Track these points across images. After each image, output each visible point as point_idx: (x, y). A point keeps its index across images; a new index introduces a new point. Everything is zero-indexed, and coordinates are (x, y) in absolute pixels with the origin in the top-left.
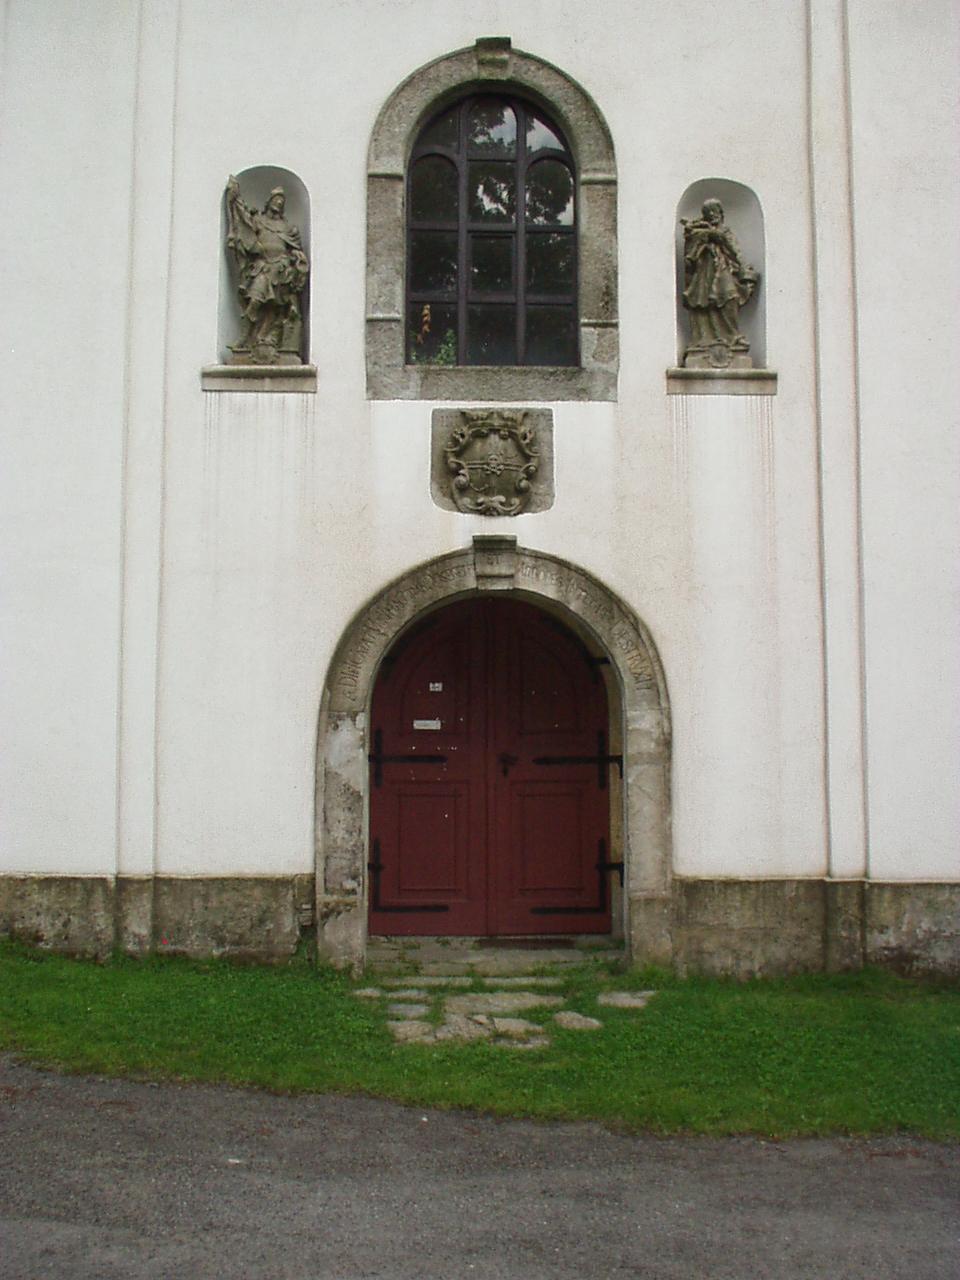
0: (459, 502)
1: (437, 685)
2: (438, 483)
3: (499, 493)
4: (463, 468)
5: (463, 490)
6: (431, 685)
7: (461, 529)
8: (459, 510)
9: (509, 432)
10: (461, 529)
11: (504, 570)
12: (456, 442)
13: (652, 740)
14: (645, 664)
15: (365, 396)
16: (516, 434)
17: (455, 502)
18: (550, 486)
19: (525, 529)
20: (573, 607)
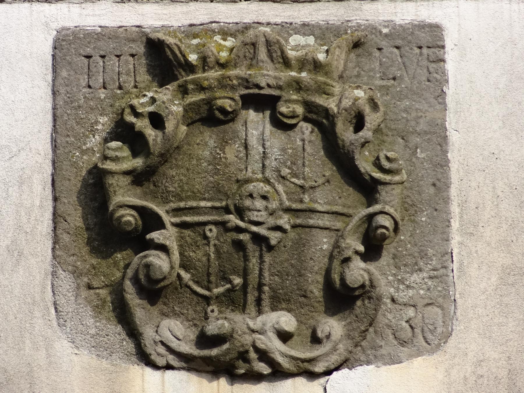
0: (148, 334)
2: (77, 273)
4: (161, 226)
5: (153, 290)
8: (145, 359)
9: (309, 106)
12: (124, 132)
17: (133, 333)
18: (441, 275)
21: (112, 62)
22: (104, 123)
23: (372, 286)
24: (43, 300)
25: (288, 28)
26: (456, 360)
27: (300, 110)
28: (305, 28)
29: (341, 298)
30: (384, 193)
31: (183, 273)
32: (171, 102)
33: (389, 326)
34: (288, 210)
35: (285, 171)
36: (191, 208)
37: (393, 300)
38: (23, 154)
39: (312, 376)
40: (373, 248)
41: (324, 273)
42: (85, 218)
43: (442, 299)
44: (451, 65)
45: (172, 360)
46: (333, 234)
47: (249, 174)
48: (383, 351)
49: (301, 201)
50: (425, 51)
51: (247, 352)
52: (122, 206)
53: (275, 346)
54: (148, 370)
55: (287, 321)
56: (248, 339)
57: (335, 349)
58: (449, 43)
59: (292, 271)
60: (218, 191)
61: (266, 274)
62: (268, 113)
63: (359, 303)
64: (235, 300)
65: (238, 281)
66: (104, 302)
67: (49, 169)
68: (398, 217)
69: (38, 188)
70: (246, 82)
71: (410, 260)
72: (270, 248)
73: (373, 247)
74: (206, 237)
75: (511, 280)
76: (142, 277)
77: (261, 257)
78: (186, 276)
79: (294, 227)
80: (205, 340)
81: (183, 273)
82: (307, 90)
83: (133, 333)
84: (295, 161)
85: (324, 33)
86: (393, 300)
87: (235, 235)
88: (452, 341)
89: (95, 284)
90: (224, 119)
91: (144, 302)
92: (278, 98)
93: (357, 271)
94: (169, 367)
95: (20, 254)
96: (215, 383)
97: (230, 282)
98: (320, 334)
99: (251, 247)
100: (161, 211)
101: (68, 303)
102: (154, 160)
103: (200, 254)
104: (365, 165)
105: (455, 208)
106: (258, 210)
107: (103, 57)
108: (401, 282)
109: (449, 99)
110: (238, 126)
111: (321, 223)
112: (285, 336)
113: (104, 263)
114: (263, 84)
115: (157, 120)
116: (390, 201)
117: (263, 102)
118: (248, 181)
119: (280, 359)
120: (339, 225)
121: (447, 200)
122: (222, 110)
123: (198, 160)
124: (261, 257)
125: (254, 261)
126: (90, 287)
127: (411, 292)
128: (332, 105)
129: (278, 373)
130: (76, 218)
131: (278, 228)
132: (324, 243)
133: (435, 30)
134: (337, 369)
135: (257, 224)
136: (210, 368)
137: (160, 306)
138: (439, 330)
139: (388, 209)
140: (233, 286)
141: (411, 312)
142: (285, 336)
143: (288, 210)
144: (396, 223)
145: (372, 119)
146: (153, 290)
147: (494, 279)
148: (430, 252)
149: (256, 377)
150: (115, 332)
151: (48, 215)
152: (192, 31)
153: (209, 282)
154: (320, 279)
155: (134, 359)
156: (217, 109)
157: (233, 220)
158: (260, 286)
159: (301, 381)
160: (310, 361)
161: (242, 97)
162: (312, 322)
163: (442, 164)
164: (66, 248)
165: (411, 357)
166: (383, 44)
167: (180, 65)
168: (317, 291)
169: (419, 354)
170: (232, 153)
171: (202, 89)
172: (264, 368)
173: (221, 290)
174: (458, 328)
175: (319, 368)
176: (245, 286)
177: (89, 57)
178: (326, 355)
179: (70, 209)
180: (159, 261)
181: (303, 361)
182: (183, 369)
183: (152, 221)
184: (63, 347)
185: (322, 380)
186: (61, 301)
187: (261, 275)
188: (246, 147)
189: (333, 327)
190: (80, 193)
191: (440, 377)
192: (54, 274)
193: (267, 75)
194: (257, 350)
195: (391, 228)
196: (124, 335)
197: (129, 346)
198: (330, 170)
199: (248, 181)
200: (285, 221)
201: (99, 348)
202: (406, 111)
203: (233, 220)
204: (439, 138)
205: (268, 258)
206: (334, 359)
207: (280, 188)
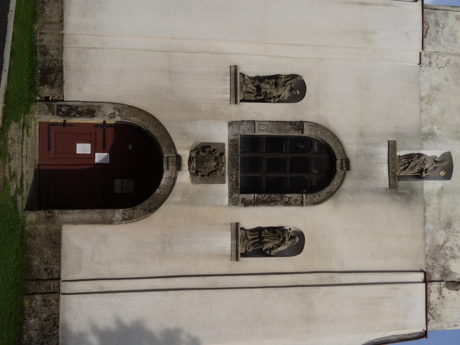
5: (198, 153)
8: (191, 152)
11: (170, 167)
12: (214, 150)
15: (229, 121)
18: (199, 183)
19: (184, 177)
20: (158, 191)
22: (216, 148)
25: (225, 167)
28: (225, 169)
29: (197, 172)
40: (202, 176)
43: (197, 183)
44: (221, 185)
53: (192, 165)
55: (195, 166)
64: (197, 161)
73: (202, 176)
80: (193, 158)
83: (193, 151)
84: (211, 168)
85: (225, 171)
90: (286, 247)
93: (200, 174)
104: (211, 175)
112: (193, 166)
115: (216, 153)
116: (207, 177)
117: (217, 165)
129: (189, 165)
130: (205, 145)
133: (225, 183)
142: (193, 166)
145: (216, 176)
146: (198, 153)
149: (189, 163)
150: (194, 149)
152: (225, 158)
156: (240, 74)
168: (198, 170)
170: (212, 161)
180: (201, 153)
183: (205, 152)
184: (192, 143)
189: (194, 171)
193: (220, 165)
198: (210, 171)
201: (192, 147)
204: (214, 183)
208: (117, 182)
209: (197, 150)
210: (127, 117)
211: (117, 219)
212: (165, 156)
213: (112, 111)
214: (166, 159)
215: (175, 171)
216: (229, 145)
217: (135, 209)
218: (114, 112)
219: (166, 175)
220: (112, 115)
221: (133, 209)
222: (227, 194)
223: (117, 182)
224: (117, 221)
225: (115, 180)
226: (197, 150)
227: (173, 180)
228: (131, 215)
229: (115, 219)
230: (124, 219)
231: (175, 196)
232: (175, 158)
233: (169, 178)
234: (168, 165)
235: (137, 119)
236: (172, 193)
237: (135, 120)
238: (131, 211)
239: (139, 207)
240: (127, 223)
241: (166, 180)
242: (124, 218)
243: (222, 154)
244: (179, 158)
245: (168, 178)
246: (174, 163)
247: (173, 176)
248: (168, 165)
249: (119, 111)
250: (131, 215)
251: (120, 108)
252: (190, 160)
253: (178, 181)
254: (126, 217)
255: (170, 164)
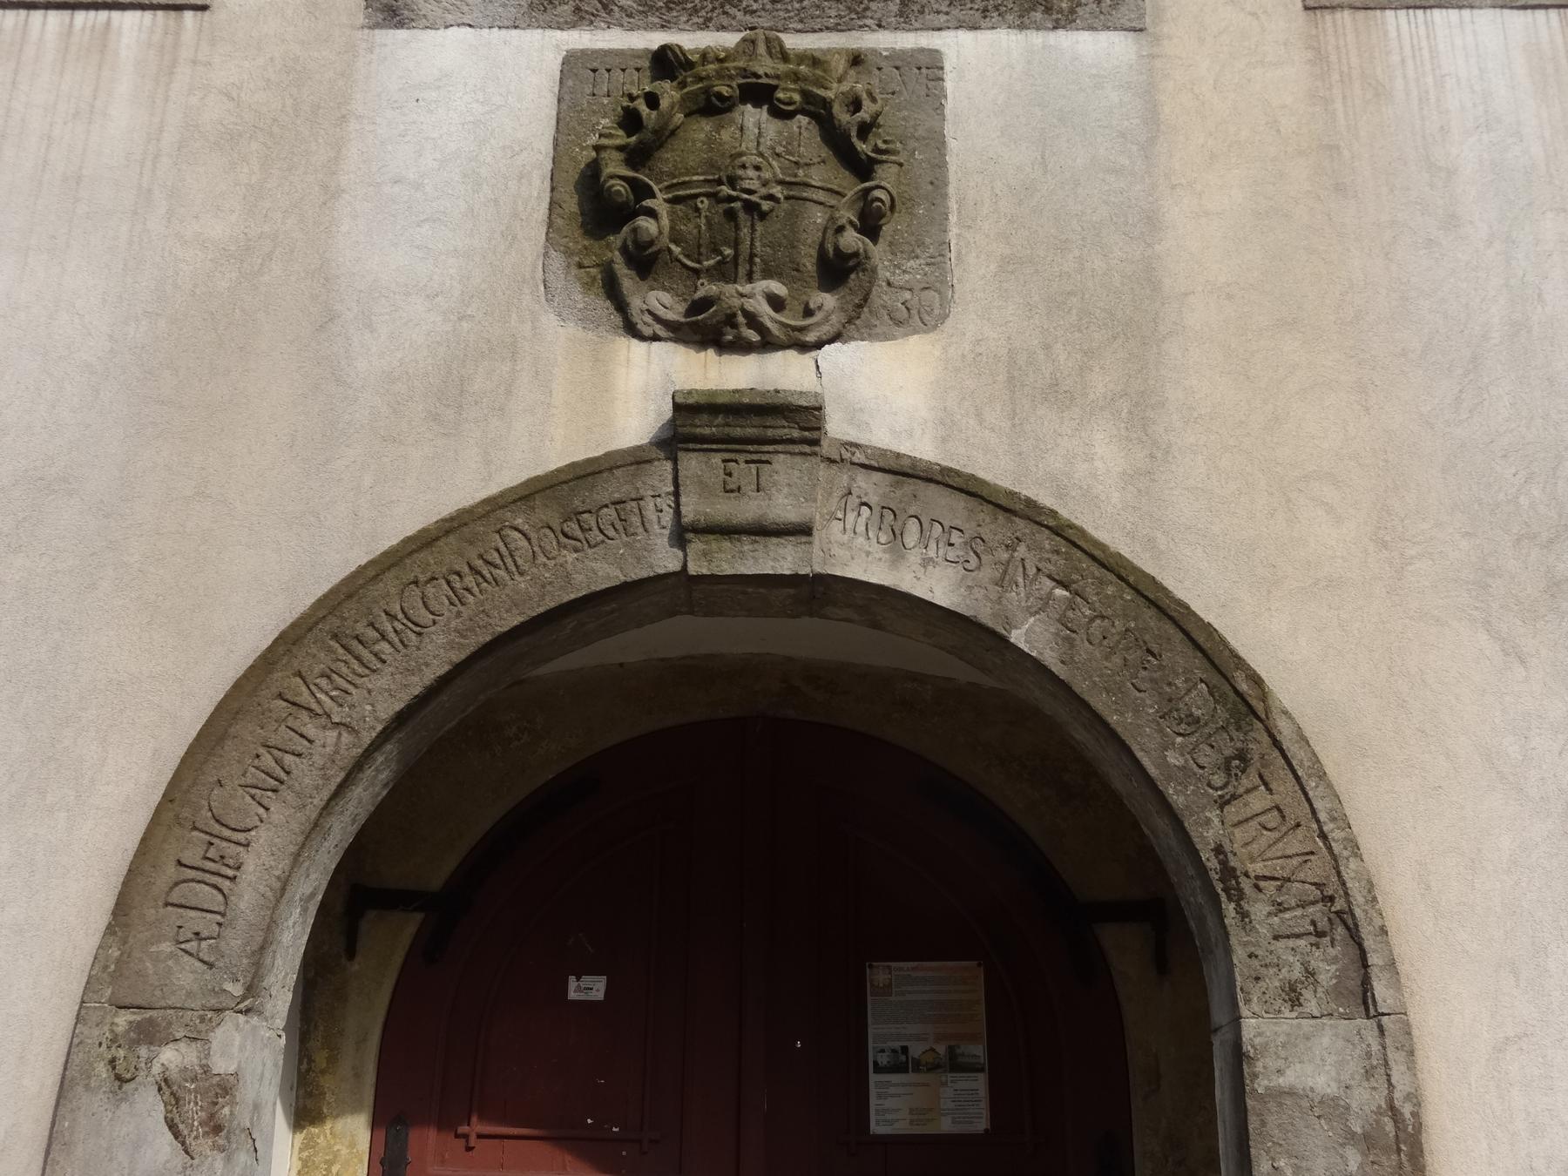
0: (635, 303)
1: (587, 980)
2: (568, 253)
3: (768, 274)
4: (653, 196)
5: (645, 261)
6: (572, 982)
7: (643, 382)
8: (632, 330)
9: (806, 95)
10: (643, 382)
11: (783, 508)
12: (630, 120)
13: (1351, 1137)
14: (1294, 844)
15: (361, 19)
16: (826, 104)
17: (621, 306)
18: (939, 259)
19: (877, 388)
20: (1030, 635)
21: (617, 74)
23: (867, 258)
24: (533, 278)
26: (954, 339)
27: (797, 97)
29: (837, 270)
30: (881, 171)
31: (673, 247)
32: (669, 93)
33: (884, 307)
34: (781, 182)
35: (779, 149)
36: (684, 183)
37: (889, 284)
38: (525, 154)
39: (804, 347)
41: (946, 1126)
42: (580, 204)
43: (938, 283)
44: (949, 85)
45: (660, 330)
46: (829, 211)
47: (743, 147)
48: (878, 330)
49: (796, 176)
50: (924, 71)
51: (734, 315)
52: (612, 177)
54: (635, 342)
56: (736, 302)
57: (826, 319)
58: (947, 66)
59: (784, 242)
60: (712, 165)
61: (758, 244)
62: (765, 107)
63: (853, 276)
64: (725, 272)
65: (728, 251)
66: (594, 279)
67: (549, 166)
68: (894, 193)
69: (537, 182)
70: (744, 73)
71: (906, 248)
72: (763, 216)
74: (697, 210)
75: (1010, 268)
76: (629, 243)
77: (753, 226)
78: (676, 249)
79: (787, 198)
81: (673, 247)
82: (805, 79)
83: (621, 306)
86: (889, 284)
87: (726, 206)
88: (949, 322)
89: (586, 263)
91: (633, 273)
92: (776, 87)
94: (655, 338)
95: (514, 238)
96: (703, 354)
97: (721, 253)
98: (812, 306)
99: (742, 215)
100: (655, 188)
101: (558, 282)
102: (647, 135)
103: (691, 226)
105: (953, 205)
106: (751, 179)
107: (608, 71)
108: (898, 266)
109: (947, 111)
110: (736, 115)
111: (815, 197)
113: (596, 244)
114: (761, 72)
116: (886, 176)
117: (758, 93)
118: (741, 154)
119: (769, 324)
120: (833, 202)
121: (945, 196)
122: (719, 96)
123: (694, 141)
124: (753, 226)
125: (745, 232)
126: (580, 266)
127: (907, 277)
128: (830, 94)
129: (768, 344)
130: (572, 204)
131: (771, 197)
132: (819, 217)
134: (831, 341)
135: (750, 192)
136: (698, 337)
137: (650, 281)
138: (936, 312)
139: (883, 184)
140: (724, 257)
141: (907, 295)
142: (776, 303)
143: (781, 182)
144: (892, 200)
147: (993, 267)
148: (928, 240)
150: (604, 306)
151: (545, 205)
153: (700, 254)
154: (814, 253)
155: (621, 331)
157: (726, 190)
158: (752, 256)
159: (791, 354)
160: (801, 329)
161: (739, 86)
162: (804, 298)
163: (941, 165)
164: (558, 231)
165: (906, 335)
166: (883, 64)
167: (681, 64)
168: (809, 265)
169: (915, 332)
171: (701, 79)
172: (754, 337)
173: (712, 262)
174: (955, 310)
175: (811, 337)
176: (736, 257)
177: (594, 71)
178: (818, 324)
179: (567, 197)
181: (794, 329)
182: (670, 339)
184: (549, 321)
185: (813, 354)
186: (551, 277)
187: (752, 244)
188: (742, 129)
190: (577, 183)
191: (937, 353)
192: (546, 255)
194: (746, 314)
195: (888, 203)
196: (612, 309)
197: (617, 319)
199: (741, 154)
200: (777, 191)
201: (586, 321)
202: (904, 119)
203: (726, 190)
204: (937, 143)
205: (759, 227)
206: (826, 330)
207: (774, 163)
208: (892, 1107)
209: (621, 269)
210: (234, 942)
211: (1354, 1067)
212: (667, 560)
213: (148, 1106)
214: (696, 545)
215: (823, 472)
216: (580, 18)
217: (1228, 873)
218: (165, 1084)
219: (856, 553)
220: (194, 1111)
221: (1238, 896)
222: (1036, 38)
223: (892, 1107)
224: (1377, 1069)
225: (877, 1128)
226: (621, 269)
227: (911, 486)
228: (1296, 919)
229: (1364, 1099)
230: (1360, 995)
231: (1088, 476)
232: (692, 463)
233: (891, 522)
234: (763, 531)
235: (261, 837)
236: (1046, 499)
237: (278, 879)
238: (1259, 910)
239: (1208, 830)
240: (1392, 965)
241: (914, 557)
242: (1337, 992)
243: (665, 62)
244: (695, 425)
245: (897, 535)
246: (743, 472)
247: (869, 486)
248: (763, 531)
249: (150, 1034)
250: (1296, 919)
251: (123, 1020)
252: (708, 329)
253: (924, 449)
254: (1327, 973)
255: (747, 509)
